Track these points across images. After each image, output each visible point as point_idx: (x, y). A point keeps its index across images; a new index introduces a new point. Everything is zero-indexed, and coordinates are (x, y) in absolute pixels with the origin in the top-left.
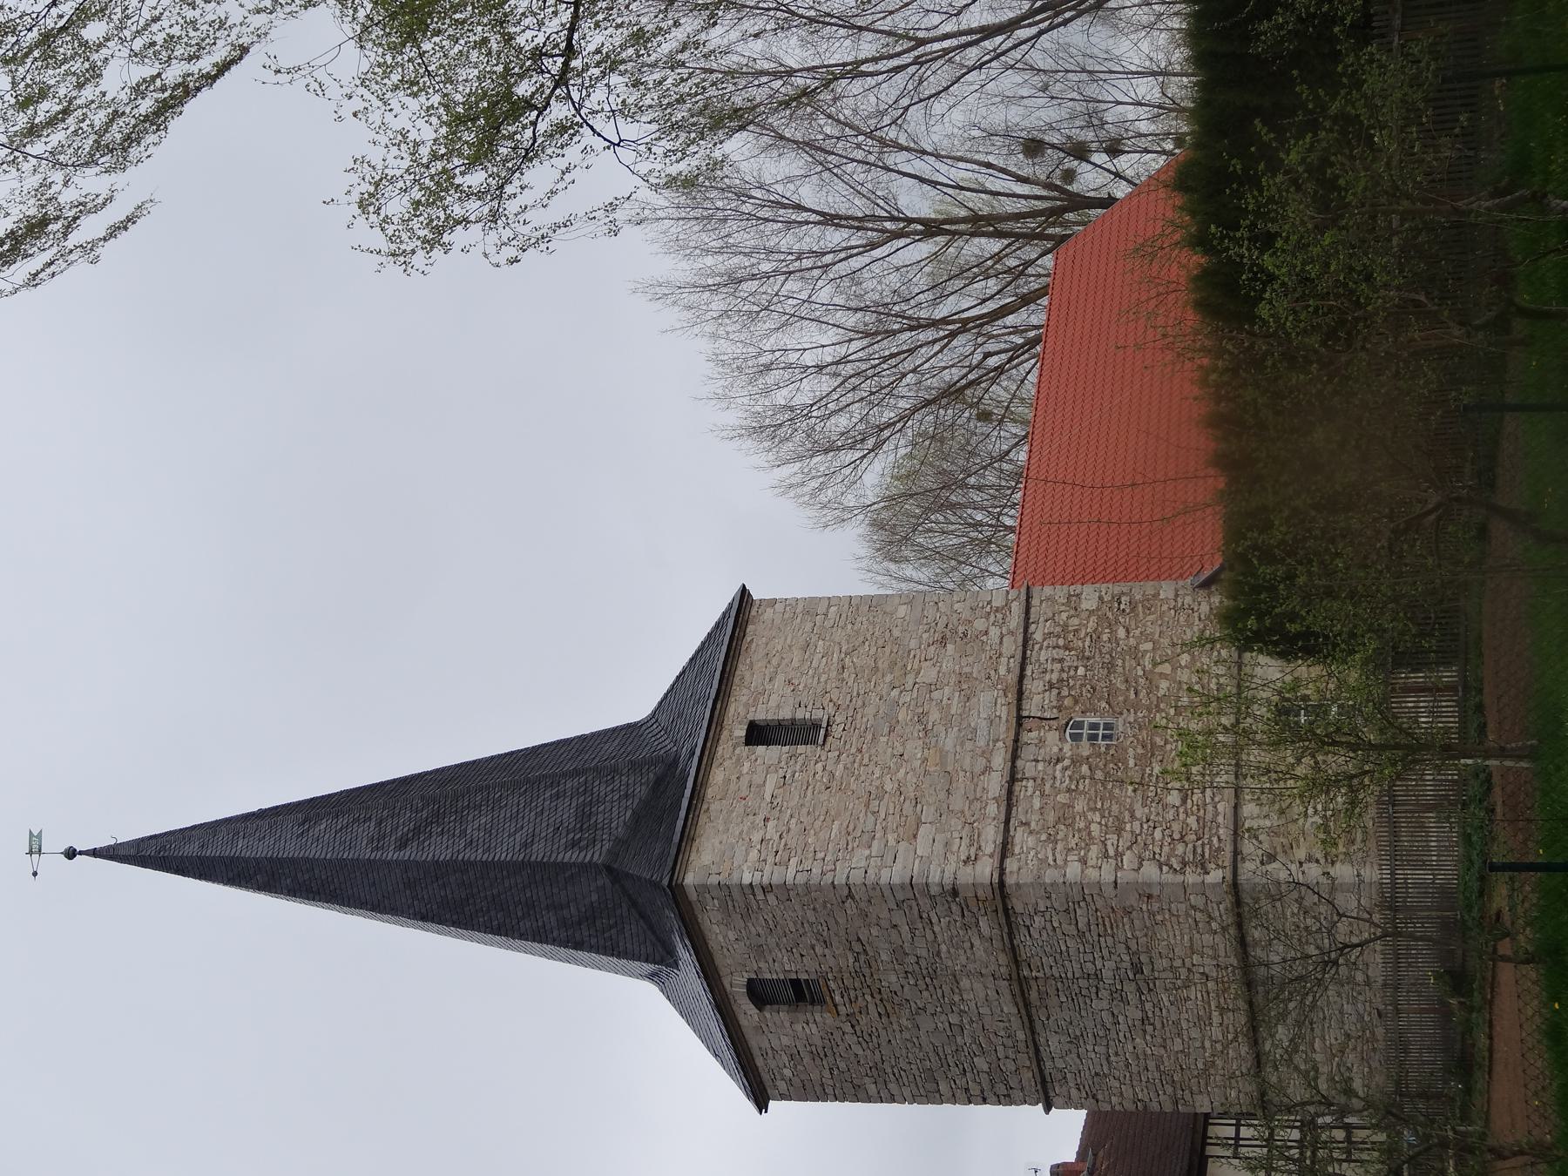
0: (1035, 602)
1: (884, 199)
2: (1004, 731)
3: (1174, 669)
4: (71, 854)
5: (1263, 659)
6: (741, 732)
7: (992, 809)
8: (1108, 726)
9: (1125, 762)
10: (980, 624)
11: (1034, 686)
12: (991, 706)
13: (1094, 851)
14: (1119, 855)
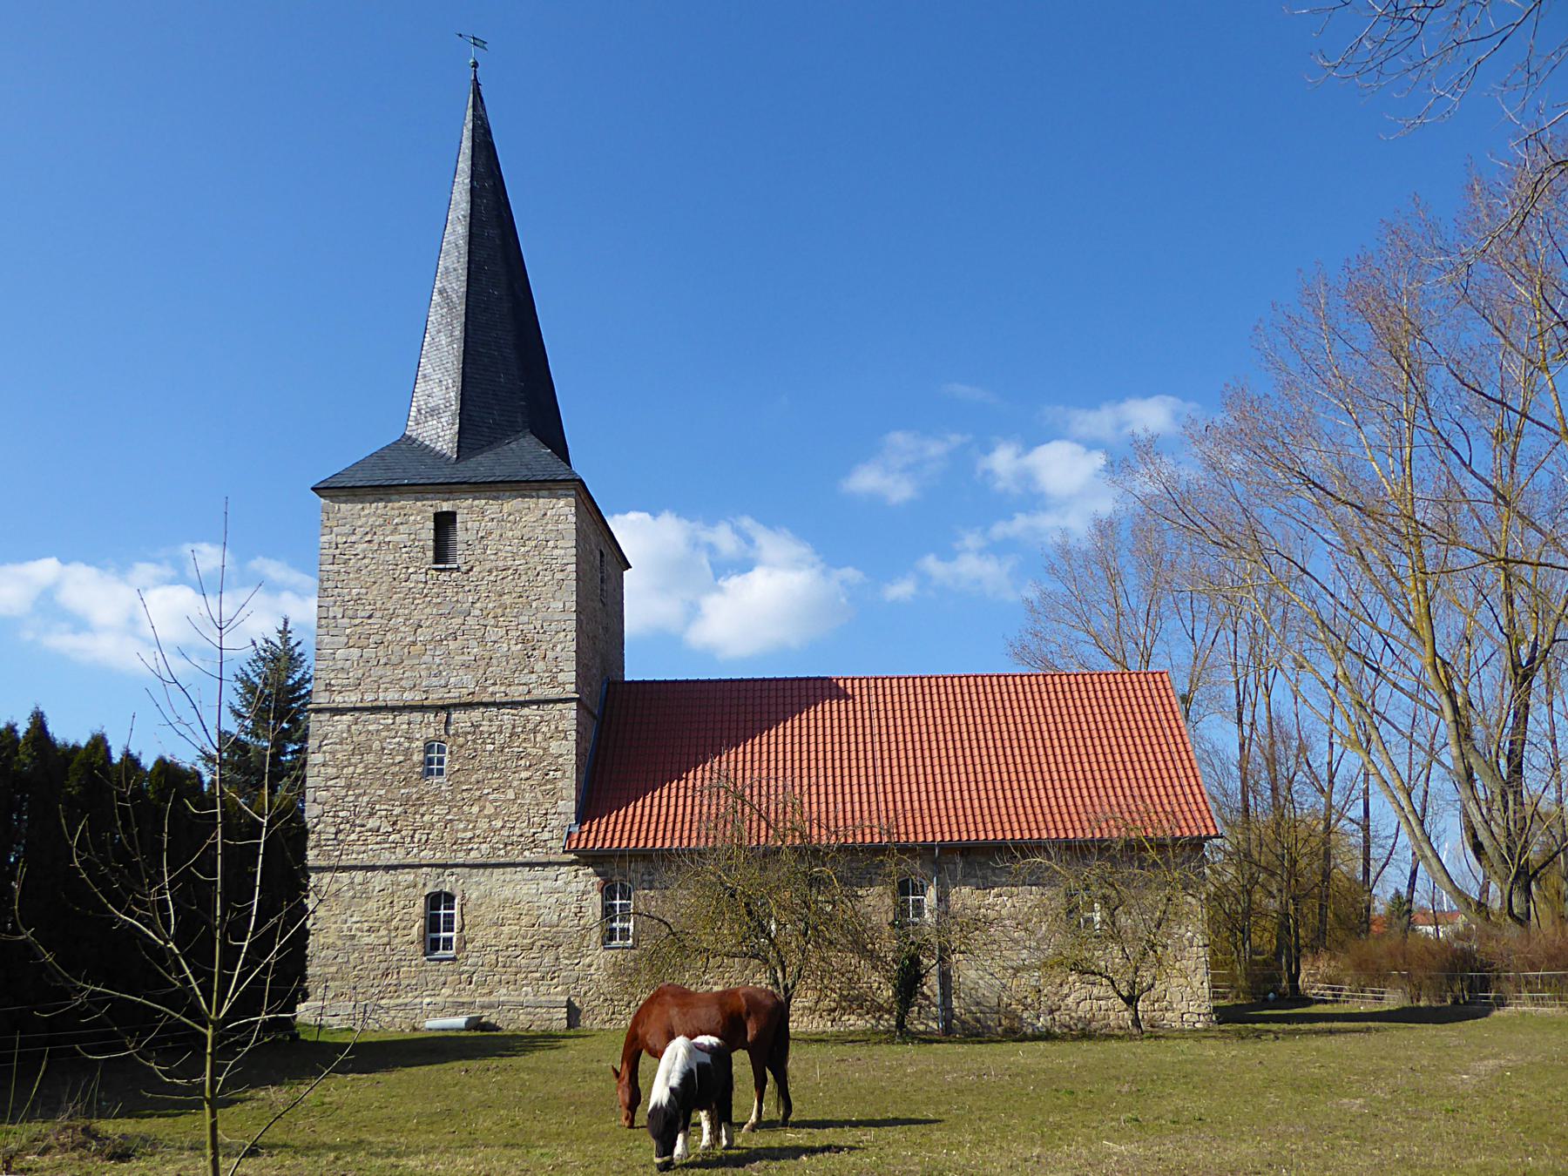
0: (560, 706)
1: (1444, 663)
2: (434, 698)
3: (488, 816)
4: (475, 65)
5: (966, 890)
6: (446, 507)
7: (369, 697)
8: (440, 772)
9: (405, 787)
10: (540, 666)
11: (476, 715)
12: (462, 684)
13: (331, 771)
14: (327, 789)
